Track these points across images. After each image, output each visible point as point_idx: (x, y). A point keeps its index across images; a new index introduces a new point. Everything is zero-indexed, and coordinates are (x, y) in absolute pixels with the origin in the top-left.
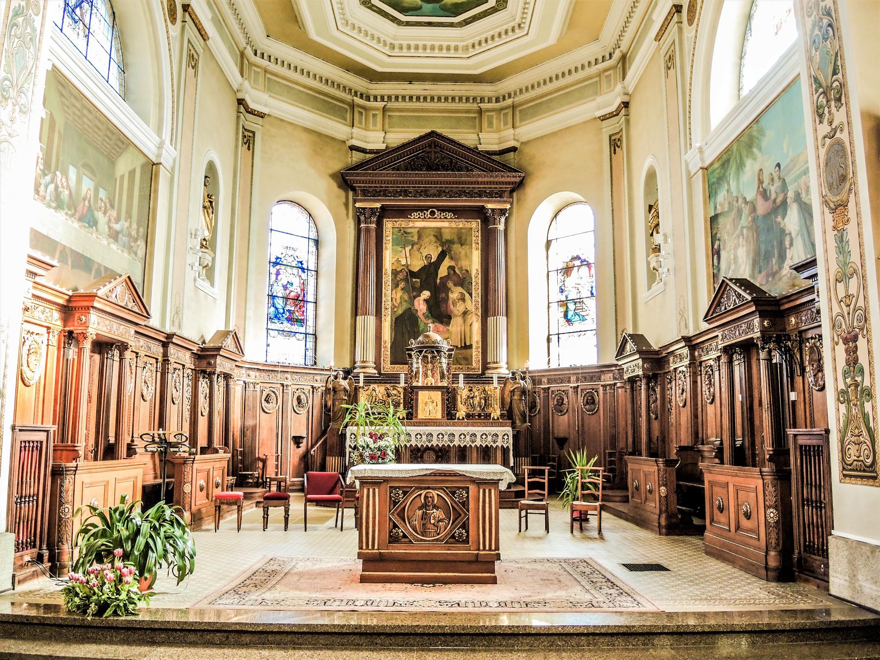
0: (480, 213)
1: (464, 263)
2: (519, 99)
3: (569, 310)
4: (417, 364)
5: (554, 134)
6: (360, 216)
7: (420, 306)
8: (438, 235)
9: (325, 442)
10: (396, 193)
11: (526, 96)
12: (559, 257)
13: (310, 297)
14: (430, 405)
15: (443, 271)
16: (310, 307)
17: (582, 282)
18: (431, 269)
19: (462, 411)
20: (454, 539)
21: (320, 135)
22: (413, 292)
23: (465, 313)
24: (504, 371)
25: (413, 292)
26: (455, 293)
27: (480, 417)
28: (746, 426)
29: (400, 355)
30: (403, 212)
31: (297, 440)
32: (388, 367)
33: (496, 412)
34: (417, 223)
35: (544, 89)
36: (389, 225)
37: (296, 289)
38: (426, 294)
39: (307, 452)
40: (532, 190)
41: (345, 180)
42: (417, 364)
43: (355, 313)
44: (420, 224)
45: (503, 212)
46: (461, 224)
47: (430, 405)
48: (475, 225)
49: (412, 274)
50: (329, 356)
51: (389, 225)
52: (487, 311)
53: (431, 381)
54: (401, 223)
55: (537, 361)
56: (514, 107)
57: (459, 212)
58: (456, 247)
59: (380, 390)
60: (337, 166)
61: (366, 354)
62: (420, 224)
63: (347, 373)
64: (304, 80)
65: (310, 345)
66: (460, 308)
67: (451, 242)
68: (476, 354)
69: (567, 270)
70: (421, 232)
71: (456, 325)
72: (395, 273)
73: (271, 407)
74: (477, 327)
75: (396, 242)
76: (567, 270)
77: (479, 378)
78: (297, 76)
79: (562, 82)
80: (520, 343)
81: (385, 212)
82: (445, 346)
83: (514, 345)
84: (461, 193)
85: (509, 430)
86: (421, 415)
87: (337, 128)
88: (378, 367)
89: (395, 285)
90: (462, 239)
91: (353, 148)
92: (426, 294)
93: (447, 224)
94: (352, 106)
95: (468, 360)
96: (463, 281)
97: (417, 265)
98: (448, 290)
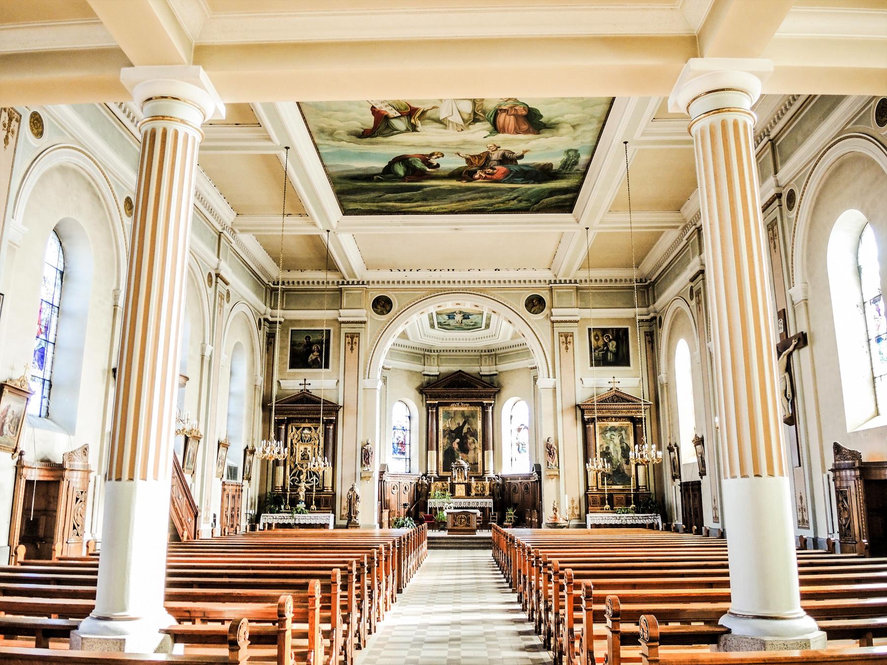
0: (481, 404)
1: (474, 426)
2: (498, 352)
3: (520, 448)
4: (455, 473)
5: (512, 371)
6: (428, 406)
7: (455, 446)
8: (463, 413)
9: (418, 505)
10: (444, 397)
11: (502, 351)
12: (516, 424)
13: (407, 442)
14: (460, 490)
15: (465, 430)
16: (407, 447)
17: (524, 437)
18: (460, 429)
19: (473, 493)
20: (467, 526)
21: (411, 371)
22: (452, 440)
23: (475, 449)
24: (492, 475)
25: (452, 440)
26: (470, 440)
27: (481, 495)
28: (558, 537)
29: (447, 468)
30: (448, 404)
31: (405, 505)
32: (442, 473)
33: (487, 493)
34: (454, 408)
35: (507, 350)
36: (441, 409)
37: (402, 440)
38: (458, 440)
39: (409, 509)
40: (504, 393)
41: (421, 390)
42: (455, 473)
43: (427, 450)
44: (455, 409)
45: (491, 404)
46: (472, 408)
47: (460, 490)
48: (479, 409)
49: (452, 431)
50: (417, 470)
51: (441, 409)
52: (485, 447)
53: (461, 480)
54: (447, 408)
55: (507, 470)
56: (496, 355)
57: (471, 404)
58: (471, 419)
59: (439, 484)
60: (418, 384)
61: (432, 467)
62: (455, 409)
63: (425, 475)
64: (403, 349)
65: (408, 463)
66: (473, 446)
67: (468, 417)
68: (480, 466)
69: (519, 430)
70: (455, 412)
71: (471, 454)
72: (444, 431)
73: (395, 491)
74: (480, 454)
75: (444, 417)
76: (519, 430)
77: (480, 478)
78: (400, 348)
79: (517, 348)
80: (498, 462)
81: (440, 404)
82: (466, 466)
83: (496, 460)
84: (472, 397)
85: (491, 500)
86: (457, 495)
87: (417, 367)
88: (437, 473)
89: (444, 437)
90: (473, 415)
91: (425, 375)
92: (458, 440)
93: (466, 409)
94: (424, 355)
95: (476, 469)
96: (474, 434)
97: (454, 428)
98: (467, 438)
